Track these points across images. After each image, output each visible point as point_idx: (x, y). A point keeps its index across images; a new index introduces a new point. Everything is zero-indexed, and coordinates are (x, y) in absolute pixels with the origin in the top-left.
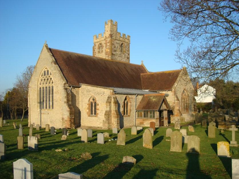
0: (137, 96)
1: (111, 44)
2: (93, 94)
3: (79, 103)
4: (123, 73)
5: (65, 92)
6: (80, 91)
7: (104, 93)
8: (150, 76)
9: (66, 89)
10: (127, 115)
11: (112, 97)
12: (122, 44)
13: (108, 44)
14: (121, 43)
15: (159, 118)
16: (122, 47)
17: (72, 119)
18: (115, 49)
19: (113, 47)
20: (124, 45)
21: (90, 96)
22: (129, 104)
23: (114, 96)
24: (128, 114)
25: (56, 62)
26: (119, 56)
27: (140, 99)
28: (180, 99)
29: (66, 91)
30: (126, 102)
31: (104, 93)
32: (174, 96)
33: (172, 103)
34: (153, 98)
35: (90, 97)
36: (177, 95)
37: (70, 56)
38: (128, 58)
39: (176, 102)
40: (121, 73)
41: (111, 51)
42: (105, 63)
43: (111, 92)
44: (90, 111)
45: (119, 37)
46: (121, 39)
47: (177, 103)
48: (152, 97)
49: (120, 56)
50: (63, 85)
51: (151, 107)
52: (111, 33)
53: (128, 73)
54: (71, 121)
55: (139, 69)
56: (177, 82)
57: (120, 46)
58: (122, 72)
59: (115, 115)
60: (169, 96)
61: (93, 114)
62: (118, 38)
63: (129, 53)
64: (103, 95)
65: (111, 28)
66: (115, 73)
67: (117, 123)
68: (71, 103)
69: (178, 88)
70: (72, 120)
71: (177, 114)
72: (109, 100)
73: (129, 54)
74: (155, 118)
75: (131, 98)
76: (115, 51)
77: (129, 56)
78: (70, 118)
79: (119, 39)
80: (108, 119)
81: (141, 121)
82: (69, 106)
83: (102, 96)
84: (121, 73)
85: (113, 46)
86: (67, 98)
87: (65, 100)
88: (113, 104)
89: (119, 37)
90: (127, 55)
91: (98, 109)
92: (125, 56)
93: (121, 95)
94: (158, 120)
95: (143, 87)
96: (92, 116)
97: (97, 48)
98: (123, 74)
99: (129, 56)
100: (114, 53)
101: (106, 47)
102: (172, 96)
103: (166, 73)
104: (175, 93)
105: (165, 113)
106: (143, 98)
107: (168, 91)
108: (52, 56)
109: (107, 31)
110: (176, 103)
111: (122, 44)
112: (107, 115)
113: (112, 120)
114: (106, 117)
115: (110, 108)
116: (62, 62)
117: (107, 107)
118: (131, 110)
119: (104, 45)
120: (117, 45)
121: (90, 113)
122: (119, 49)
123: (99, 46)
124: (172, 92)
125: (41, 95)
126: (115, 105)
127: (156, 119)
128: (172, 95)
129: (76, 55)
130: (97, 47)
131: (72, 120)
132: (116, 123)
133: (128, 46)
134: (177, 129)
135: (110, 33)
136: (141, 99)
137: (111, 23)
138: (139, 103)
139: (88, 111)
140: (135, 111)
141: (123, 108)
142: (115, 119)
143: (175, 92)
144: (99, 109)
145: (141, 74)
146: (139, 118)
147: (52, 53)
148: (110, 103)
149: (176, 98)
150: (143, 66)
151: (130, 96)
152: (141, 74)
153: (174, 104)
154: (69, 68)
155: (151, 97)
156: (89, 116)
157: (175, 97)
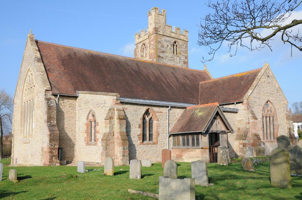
0: (171, 109)
1: (156, 42)
2: (92, 107)
3: (75, 124)
4: (168, 80)
5: (46, 104)
6: (77, 104)
7: (105, 103)
8: (212, 84)
9: (48, 100)
10: (151, 142)
11: (115, 109)
12: (175, 42)
13: (152, 43)
14: (174, 40)
15: (208, 147)
16: (175, 47)
17: (54, 149)
18: (163, 49)
19: (159, 46)
20: (179, 43)
21: (89, 110)
22: (155, 122)
23: (121, 107)
24: (154, 141)
25: (42, 59)
26: (170, 60)
27: (178, 114)
28: (259, 116)
29: (48, 103)
30: (147, 119)
31: (105, 103)
32: (246, 112)
33: (245, 123)
34: (200, 111)
35: (88, 112)
36: (253, 109)
37: (75, 53)
38: (186, 63)
39: (251, 120)
40: (164, 80)
41: (156, 53)
42: (137, 65)
43: (114, 99)
44: (89, 136)
45: (169, 33)
46: (173, 35)
47: (252, 122)
48: (198, 111)
49: (172, 60)
50: (44, 93)
51: (192, 126)
52: (155, 25)
53: (178, 81)
54: (51, 152)
55: (200, 76)
56: (252, 87)
57: (171, 45)
58: (165, 78)
59: (118, 140)
60: (239, 112)
61: (93, 141)
62: (168, 33)
63: (187, 56)
64: (104, 106)
65: (155, 19)
66: (152, 79)
67: (123, 156)
68: (56, 122)
69: (254, 97)
70: (56, 152)
71: (254, 141)
72: (110, 113)
73: (186, 57)
74: (200, 147)
75: (158, 112)
76: (163, 52)
77: (186, 59)
78: (50, 148)
79: (169, 36)
80: (106, 148)
81: (178, 153)
82: (51, 127)
83: (102, 108)
84: (164, 80)
85: (160, 44)
86: (48, 113)
87: (45, 117)
88: (116, 121)
89: (170, 31)
90: (183, 58)
91: (98, 132)
92: (180, 59)
93: (135, 106)
94: (208, 151)
95: (201, 100)
96: (90, 145)
97: (139, 52)
98: (168, 82)
99: (188, 60)
100: (161, 55)
101: (150, 47)
102: (244, 111)
103: (236, 77)
104: (249, 106)
105: (222, 137)
106: (184, 112)
107: (237, 105)
108: (36, 50)
109: (151, 24)
110: (251, 124)
111: (175, 42)
112: (104, 140)
113: (115, 150)
114: (103, 144)
115: (112, 127)
116: (56, 60)
117: (106, 128)
118: (158, 134)
119: (148, 45)
120: (165, 44)
121: (89, 139)
122: (170, 49)
123: (143, 48)
124: (244, 104)
125: (149, 134)
126: (120, 122)
127: (202, 148)
128: (244, 110)
129: (87, 53)
130: (139, 49)
131: (54, 151)
132: (120, 155)
133: (185, 45)
134: (222, 164)
135: (154, 27)
136: (180, 115)
137: (155, 11)
138: (176, 121)
139: (85, 135)
140: (168, 135)
141: (141, 129)
142: (119, 147)
143: (248, 104)
144: (100, 131)
145: (201, 83)
146: (174, 147)
147: (38, 46)
148: (111, 118)
149: (250, 115)
150: (206, 73)
151: (156, 109)
152: (201, 83)
153: (248, 125)
154: (65, 69)
155: (197, 109)
156: (88, 144)
157: (249, 112)
